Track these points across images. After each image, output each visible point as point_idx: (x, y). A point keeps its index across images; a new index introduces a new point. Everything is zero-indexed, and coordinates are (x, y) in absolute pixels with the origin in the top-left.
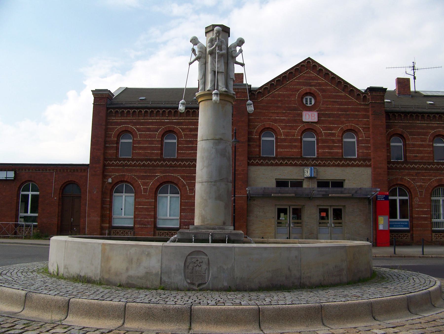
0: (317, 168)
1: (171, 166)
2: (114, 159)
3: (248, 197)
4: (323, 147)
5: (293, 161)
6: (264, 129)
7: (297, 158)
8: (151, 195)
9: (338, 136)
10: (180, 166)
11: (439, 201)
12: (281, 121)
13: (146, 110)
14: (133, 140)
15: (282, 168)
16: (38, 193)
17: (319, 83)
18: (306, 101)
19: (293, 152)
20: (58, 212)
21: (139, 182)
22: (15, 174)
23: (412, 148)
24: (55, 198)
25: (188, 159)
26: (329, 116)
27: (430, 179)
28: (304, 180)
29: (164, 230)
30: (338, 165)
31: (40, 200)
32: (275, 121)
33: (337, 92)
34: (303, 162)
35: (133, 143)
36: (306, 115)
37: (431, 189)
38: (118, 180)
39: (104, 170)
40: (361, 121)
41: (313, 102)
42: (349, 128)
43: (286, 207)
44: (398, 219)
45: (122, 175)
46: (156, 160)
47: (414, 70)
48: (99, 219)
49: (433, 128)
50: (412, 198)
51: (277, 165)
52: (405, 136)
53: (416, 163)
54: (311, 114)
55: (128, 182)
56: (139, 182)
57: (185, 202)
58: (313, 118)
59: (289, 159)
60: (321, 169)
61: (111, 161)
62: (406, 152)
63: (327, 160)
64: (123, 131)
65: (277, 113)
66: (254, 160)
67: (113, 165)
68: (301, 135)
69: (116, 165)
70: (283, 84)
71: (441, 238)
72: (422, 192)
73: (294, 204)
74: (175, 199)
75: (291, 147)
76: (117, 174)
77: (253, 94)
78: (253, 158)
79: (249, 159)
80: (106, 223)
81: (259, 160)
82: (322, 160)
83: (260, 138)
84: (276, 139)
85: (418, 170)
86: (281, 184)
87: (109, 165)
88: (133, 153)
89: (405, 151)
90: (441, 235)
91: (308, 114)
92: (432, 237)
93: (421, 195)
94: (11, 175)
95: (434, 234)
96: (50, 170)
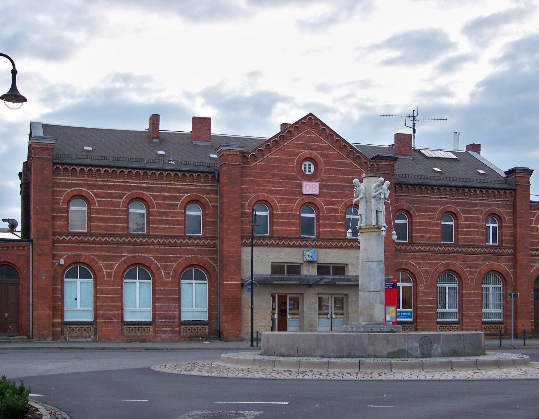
0: (318, 250)
1: (141, 244)
2: (65, 233)
4: (325, 226)
5: (291, 241)
7: (296, 238)
8: (117, 281)
9: (341, 212)
10: (153, 244)
11: (445, 288)
12: (278, 192)
13: (107, 169)
17: (321, 146)
18: (305, 168)
19: (291, 230)
21: (101, 264)
25: (163, 236)
27: (437, 264)
28: (302, 263)
29: (134, 325)
30: (341, 247)
32: (271, 192)
33: (341, 159)
36: (306, 187)
37: (438, 275)
38: (72, 262)
44: (401, 309)
45: (77, 255)
47: (414, 120)
48: (51, 313)
50: (417, 285)
51: (273, 245)
53: (422, 245)
54: (312, 185)
56: (101, 264)
57: (160, 289)
58: (314, 190)
59: (286, 239)
60: (322, 251)
61: (61, 236)
62: (412, 231)
63: (328, 240)
65: (273, 183)
66: (247, 239)
67: (64, 241)
69: (69, 242)
70: (280, 145)
72: (428, 278)
73: (292, 292)
74: (145, 285)
75: (289, 224)
76: (70, 253)
77: (245, 156)
78: (246, 237)
82: (323, 240)
85: (424, 252)
86: (277, 268)
87: (59, 241)
89: (411, 230)
90: (446, 327)
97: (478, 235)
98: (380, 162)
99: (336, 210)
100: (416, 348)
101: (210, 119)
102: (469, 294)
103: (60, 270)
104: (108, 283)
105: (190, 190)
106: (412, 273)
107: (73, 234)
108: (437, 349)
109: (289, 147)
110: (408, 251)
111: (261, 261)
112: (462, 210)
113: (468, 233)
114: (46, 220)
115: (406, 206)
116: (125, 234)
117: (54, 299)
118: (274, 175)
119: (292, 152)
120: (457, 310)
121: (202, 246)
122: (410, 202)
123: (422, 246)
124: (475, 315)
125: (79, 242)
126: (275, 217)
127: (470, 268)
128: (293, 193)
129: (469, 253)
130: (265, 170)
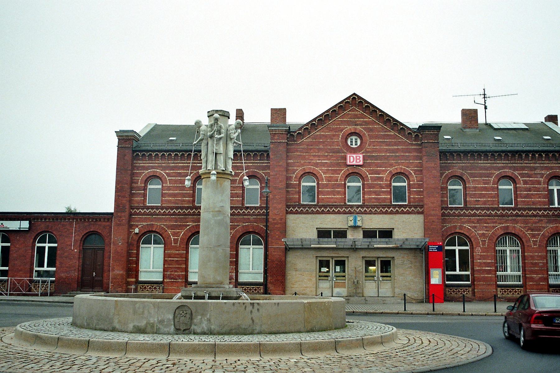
3: (286, 248)
4: (370, 193)
5: (336, 208)
6: (304, 173)
9: (386, 180)
12: (324, 165)
14: (163, 186)
15: (323, 216)
16: (56, 245)
17: (365, 122)
19: (337, 198)
20: (79, 266)
22: (30, 223)
23: (473, 191)
24: (76, 251)
26: (376, 158)
27: (494, 227)
30: (386, 213)
31: (58, 252)
32: (316, 165)
33: (386, 132)
34: (347, 210)
35: (162, 190)
39: (130, 219)
40: (413, 163)
41: (359, 143)
42: (399, 171)
43: (328, 259)
46: (187, 208)
47: (485, 98)
49: (499, 169)
51: (318, 213)
52: (464, 178)
53: (477, 209)
54: (356, 157)
55: (157, 233)
59: (331, 206)
64: (150, 177)
65: (319, 156)
68: (345, 180)
70: (326, 123)
71: (508, 294)
72: (485, 241)
75: (333, 193)
76: (145, 224)
79: (288, 206)
80: (133, 278)
81: (298, 207)
82: (368, 207)
83: (300, 183)
84: (318, 184)
86: (323, 234)
88: (162, 200)
89: (465, 195)
90: (508, 290)
91: (353, 157)
92: (497, 291)
93: (484, 244)
94: (25, 225)
95: (499, 289)
96: (69, 219)
97: (540, 197)
98: (423, 132)
99: (381, 179)
100: (169, 319)
101: (237, 110)
102: (532, 257)
103: (136, 238)
104: (175, 248)
105: (551, 168)
106: (468, 237)
107: (148, 208)
108: (201, 322)
109: (333, 124)
110: (462, 215)
111: (303, 228)
112: (520, 174)
113: (527, 196)
114: (124, 197)
115: (459, 172)
116: (191, 207)
117: (129, 262)
118: (319, 150)
119: (337, 128)
120: (520, 273)
121: (257, 215)
122: (462, 168)
123: (477, 210)
124: (540, 278)
125: (152, 214)
126: (320, 187)
127: (532, 230)
128: (338, 165)
129: (530, 216)
130: (312, 146)
